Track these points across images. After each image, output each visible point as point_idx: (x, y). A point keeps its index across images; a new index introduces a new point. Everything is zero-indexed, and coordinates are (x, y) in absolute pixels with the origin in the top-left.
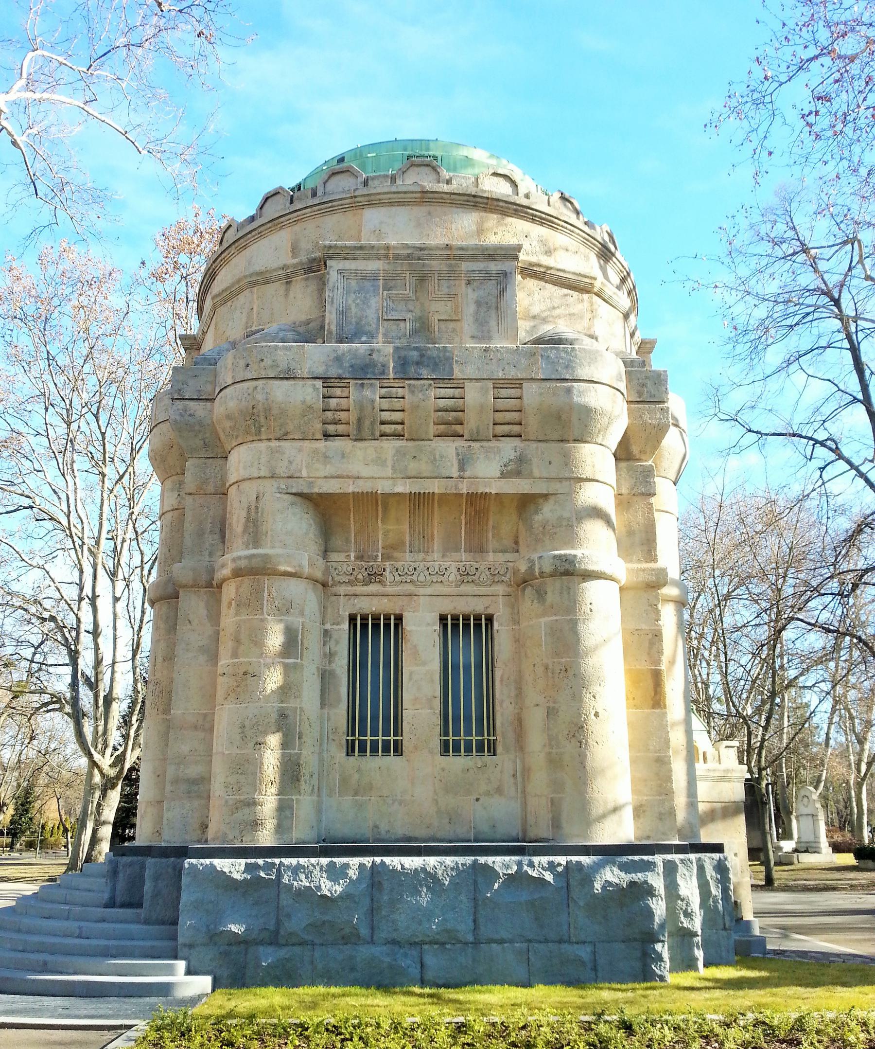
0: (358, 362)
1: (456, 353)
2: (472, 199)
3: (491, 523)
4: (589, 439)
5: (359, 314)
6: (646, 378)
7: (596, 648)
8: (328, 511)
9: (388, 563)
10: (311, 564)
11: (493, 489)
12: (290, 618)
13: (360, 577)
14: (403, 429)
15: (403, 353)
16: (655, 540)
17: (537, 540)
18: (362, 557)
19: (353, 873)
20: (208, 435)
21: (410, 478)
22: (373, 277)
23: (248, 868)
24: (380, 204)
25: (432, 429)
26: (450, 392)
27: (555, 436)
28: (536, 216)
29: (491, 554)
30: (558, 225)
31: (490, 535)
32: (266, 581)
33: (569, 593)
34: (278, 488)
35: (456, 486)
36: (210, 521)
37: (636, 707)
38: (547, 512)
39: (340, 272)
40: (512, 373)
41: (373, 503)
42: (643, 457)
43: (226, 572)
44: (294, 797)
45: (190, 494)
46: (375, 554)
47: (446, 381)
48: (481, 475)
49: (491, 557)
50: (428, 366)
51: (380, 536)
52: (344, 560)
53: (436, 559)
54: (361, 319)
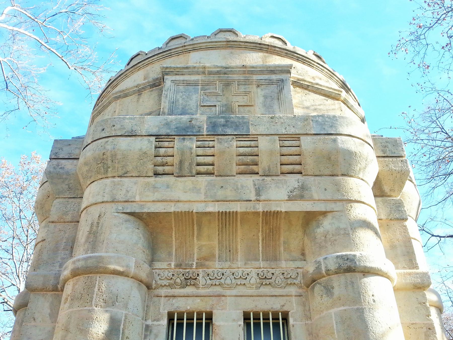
0: (182, 125)
1: (251, 119)
2: (258, 45)
3: (282, 239)
4: (353, 174)
5: (184, 103)
6: (387, 142)
7: (383, 335)
8: (151, 224)
9: (201, 270)
10: (137, 266)
11: (283, 208)
12: (115, 310)
13: (178, 281)
14: (214, 169)
15: (214, 120)
16: (413, 253)
17: (321, 247)
18: (181, 265)
20: (72, 181)
21: (218, 201)
22: (195, 84)
24: (201, 49)
25: (235, 169)
26: (248, 143)
27: (327, 172)
28: (299, 58)
29: (283, 262)
30: (314, 65)
31: (282, 249)
32: (98, 278)
33: (353, 286)
34: (116, 209)
35: (254, 206)
36: (64, 241)
38: (327, 224)
39: (173, 81)
40: (292, 131)
41: (191, 221)
43: (66, 273)
45: (53, 222)
46: (190, 263)
48: (273, 198)
49: (283, 264)
50: (232, 127)
51: (196, 251)
52: (166, 267)
53: (240, 266)
54: (185, 106)
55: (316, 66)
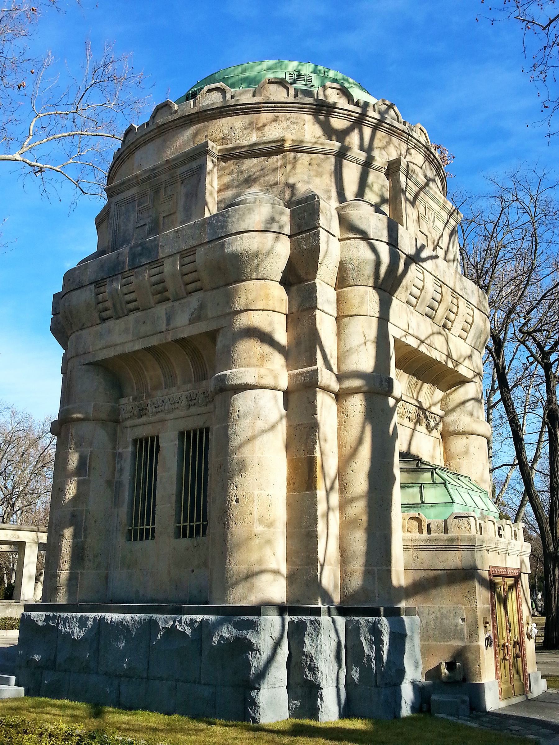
2: (187, 118)
13: (135, 413)
19: (90, 624)
23: (47, 618)
37: (295, 490)
42: (309, 277)
44: (79, 571)
47: (156, 262)
51: (149, 381)
55: (264, 107)
